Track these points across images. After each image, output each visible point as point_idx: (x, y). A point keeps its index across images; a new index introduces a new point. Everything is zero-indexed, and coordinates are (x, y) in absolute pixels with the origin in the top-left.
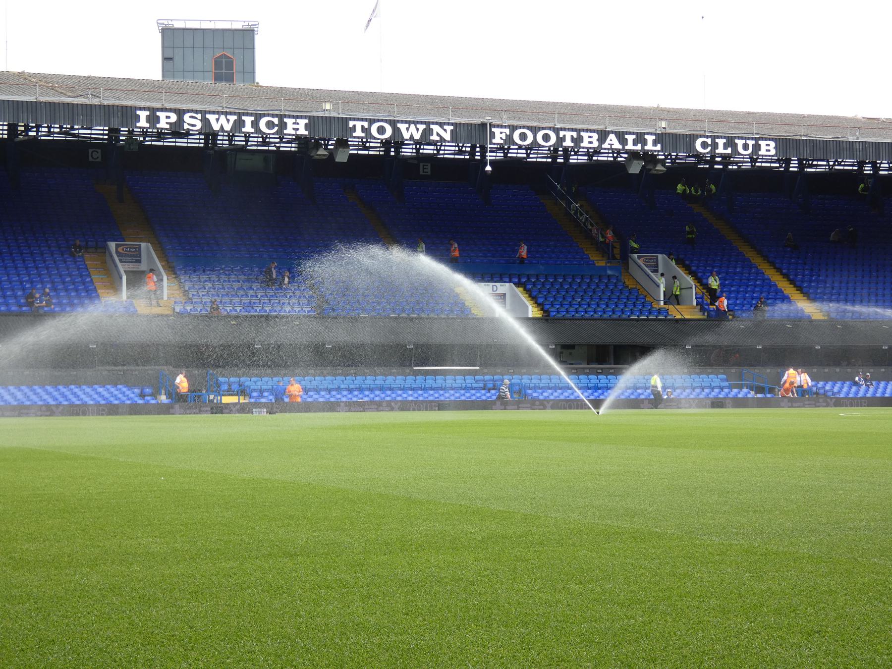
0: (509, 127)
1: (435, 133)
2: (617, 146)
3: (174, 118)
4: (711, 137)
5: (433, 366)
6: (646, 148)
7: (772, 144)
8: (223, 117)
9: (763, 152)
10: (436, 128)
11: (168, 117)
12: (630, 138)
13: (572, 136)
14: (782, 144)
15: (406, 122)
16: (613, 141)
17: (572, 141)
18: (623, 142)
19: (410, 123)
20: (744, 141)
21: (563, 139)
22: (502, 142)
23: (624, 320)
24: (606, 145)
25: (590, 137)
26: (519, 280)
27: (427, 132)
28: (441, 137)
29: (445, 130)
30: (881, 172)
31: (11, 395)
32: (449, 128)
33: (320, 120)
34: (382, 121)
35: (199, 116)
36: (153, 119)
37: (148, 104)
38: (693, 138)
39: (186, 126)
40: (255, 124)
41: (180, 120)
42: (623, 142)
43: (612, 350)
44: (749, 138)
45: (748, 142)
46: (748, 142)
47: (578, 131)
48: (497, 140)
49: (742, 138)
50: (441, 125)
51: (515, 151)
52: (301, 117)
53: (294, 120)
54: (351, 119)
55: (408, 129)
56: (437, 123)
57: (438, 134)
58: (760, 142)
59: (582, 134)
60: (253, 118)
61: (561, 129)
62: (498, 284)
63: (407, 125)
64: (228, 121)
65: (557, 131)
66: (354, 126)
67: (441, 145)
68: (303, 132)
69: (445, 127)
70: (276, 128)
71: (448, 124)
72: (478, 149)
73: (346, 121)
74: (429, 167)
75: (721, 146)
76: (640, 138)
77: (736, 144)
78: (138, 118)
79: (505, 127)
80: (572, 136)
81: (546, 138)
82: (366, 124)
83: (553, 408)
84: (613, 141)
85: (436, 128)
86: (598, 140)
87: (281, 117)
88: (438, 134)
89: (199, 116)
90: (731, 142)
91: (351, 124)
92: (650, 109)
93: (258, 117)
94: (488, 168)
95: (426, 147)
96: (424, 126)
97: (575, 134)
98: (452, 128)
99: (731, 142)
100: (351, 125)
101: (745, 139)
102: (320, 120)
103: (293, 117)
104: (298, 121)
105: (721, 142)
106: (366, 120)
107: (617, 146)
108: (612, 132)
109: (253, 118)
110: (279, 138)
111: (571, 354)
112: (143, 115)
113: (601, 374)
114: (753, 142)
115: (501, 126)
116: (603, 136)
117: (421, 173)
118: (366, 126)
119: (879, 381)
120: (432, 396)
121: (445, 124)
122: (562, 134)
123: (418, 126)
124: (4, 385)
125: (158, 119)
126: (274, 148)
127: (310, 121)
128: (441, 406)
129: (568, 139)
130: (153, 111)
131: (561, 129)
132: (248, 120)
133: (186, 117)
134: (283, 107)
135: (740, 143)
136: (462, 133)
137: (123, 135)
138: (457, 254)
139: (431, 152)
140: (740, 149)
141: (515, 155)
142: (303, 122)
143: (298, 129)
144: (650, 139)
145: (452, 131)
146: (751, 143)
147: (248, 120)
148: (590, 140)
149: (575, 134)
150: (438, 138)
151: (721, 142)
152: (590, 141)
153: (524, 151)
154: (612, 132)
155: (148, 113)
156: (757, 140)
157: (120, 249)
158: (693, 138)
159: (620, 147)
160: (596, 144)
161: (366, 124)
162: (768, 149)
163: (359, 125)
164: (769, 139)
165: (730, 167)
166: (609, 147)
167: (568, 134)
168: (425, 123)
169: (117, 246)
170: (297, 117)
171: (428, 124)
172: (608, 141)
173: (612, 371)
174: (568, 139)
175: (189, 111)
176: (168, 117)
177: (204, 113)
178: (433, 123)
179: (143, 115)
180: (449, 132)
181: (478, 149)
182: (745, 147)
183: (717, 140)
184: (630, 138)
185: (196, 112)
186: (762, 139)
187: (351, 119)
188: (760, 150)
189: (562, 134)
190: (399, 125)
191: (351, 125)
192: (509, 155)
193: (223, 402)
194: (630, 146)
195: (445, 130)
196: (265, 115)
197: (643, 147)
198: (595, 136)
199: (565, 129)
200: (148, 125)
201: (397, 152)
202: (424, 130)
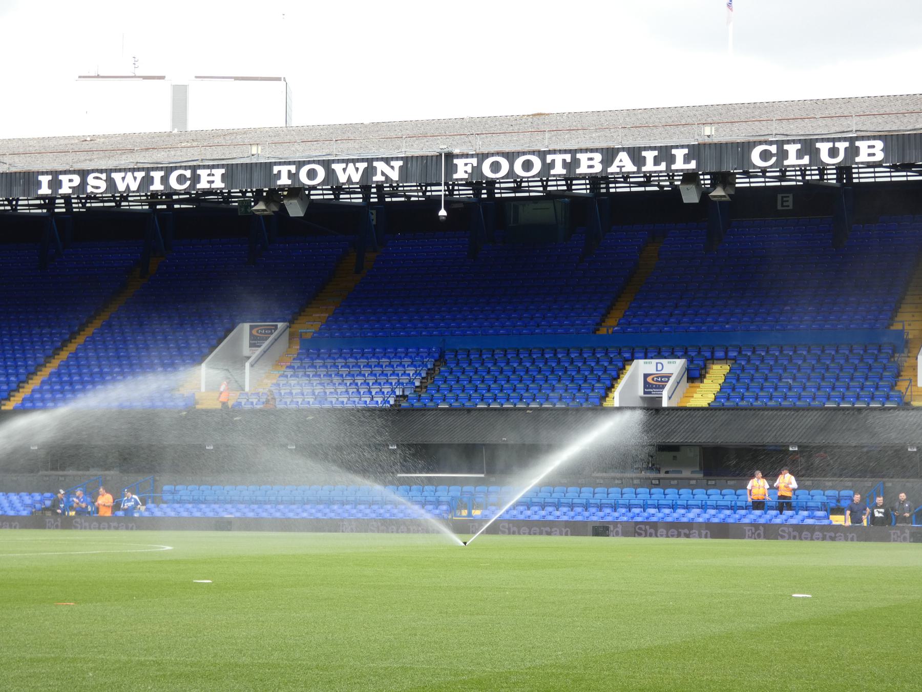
0: (477, 155)
1: (379, 172)
2: (630, 167)
3: (77, 180)
4: (776, 142)
5: (436, 472)
6: (674, 167)
7: (879, 144)
8: (129, 174)
9: (863, 157)
10: (380, 166)
11: (71, 181)
12: (650, 156)
13: (564, 161)
14: (232, 172)
15: (343, 161)
16: (624, 162)
17: (289, 178)
19: (347, 161)
20: (830, 145)
21: (552, 165)
22: (466, 176)
23: (786, 409)
24: (613, 169)
26: (726, 353)
27: (369, 171)
28: (387, 177)
29: (392, 167)
30: (56, 210)
31: (18, 503)
32: (397, 164)
33: (239, 168)
34: (314, 162)
35: (104, 176)
36: (55, 184)
37: (49, 168)
38: (748, 146)
39: (90, 189)
40: (165, 180)
41: (84, 184)
44: (839, 140)
45: (837, 145)
46: (837, 145)
47: (573, 152)
49: (828, 140)
50: (387, 161)
51: (554, 183)
52: (218, 167)
53: (208, 171)
54: (275, 164)
56: (382, 159)
57: (383, 174)
60: (162, 173)
61: (550, 152)
62: (664, 361)
63: (344, 165)
65: (542, 155)
66: (279, 172)
68: (219, 184)
69: (392, 163)
70: (774, 159)
71: (397, 159)
72: (374, 190)
73: (269, 166)
74: (791, 199)
76: (665, 154)
77: (818, 150)
78: (39, 185)
79: (472, 156)
80: (564, 161)
81: (527, 166)
82: (293, 169)
83: (626, 534)
85: (380, 166)
87: (194, 169)
88: (383, 174)
89: (104, 176)
90: (808, 147)
91: (276, 169)
92: (561, 115)
93: (169, 170)
94: (443, 213)
95: (434, 188)
96: (365, 165)
97: (568, 158)
98: (401, 163)
99: (808, 147)
100: (275, 172)
101: (833, 140)
102: (239, 168)
103: (208, 167)
104: (214, 171)
105: (792, 149)
106: (294, 163)
107: (630, 167)
108: (623, 149)
109: (162, 173)
110: (780, 171)
111: (675, 457)
112: (45, 180)
113: (656, 486)
114: (847, 144)
115: (467, 156)
116: (609, 155)
117: (779, 207)
118: (293, 171)
120: (208, 511)
121: (392, 159)
122: (549, 158)
123: (358, 165)
124: (6, 491)
125: (59, 184)
126: (656, 189)
128: (223, 525)
129: (284, 175)
130: (55, 174)
131: (550, 152)
132: (157, 175)
133: (90, 179)
134: (853, 125)
135: (824, 148)
136: (414, 168)
137: (374, 193)
139: (584, 192)
140: (825, 157)
141: (555, 188)
142: (219, 172)
143: (213, 182)
145: (401, 168)
146: (842, 146)
147: (157, 175)
148: (591, 163)
149: (568, 158)
150: (383, 179)
152: (590, 165)
153: (564, 183)
154: (623, 149)
155: (50, 177)
156: (852, 140)
157: (254, 332)
158: (748, 146)
159: (635, 169)
160: (598, 168)
161: (293, 169)
162: (871, 151)
163: (284, 170)
164: (875, 138)
165: (158, 207)
166: (618, 170)
167: (559, 159)
168: (367, 160)
169: (252, 328)
170: (213, 167)
171: (370, 161)
172: (617, 162)
173: (673, 482)
174: (284, 175)
175: (93, 171)
176: (71, 181)
177: (109, 172)
178: (377, 159)
179: (45, 180)
180: (397, 169)
181: (374, 190)
182: (833, 152)
183: (786, 147)
184: (650, 156)
185: (101, 171)
186: (863, 138)
187: (275, 164)
189: (549, 158)
190: (334, 166)
191: (275, 172)
192: (549, 188)
193: (834, 523)
194: (649, 167)
195: (392, 167)
196: (176, 168)
198: (598, 157)
199: (554, 152)
200: (223, 185)
201: (491, 193)
202: (366, 170)
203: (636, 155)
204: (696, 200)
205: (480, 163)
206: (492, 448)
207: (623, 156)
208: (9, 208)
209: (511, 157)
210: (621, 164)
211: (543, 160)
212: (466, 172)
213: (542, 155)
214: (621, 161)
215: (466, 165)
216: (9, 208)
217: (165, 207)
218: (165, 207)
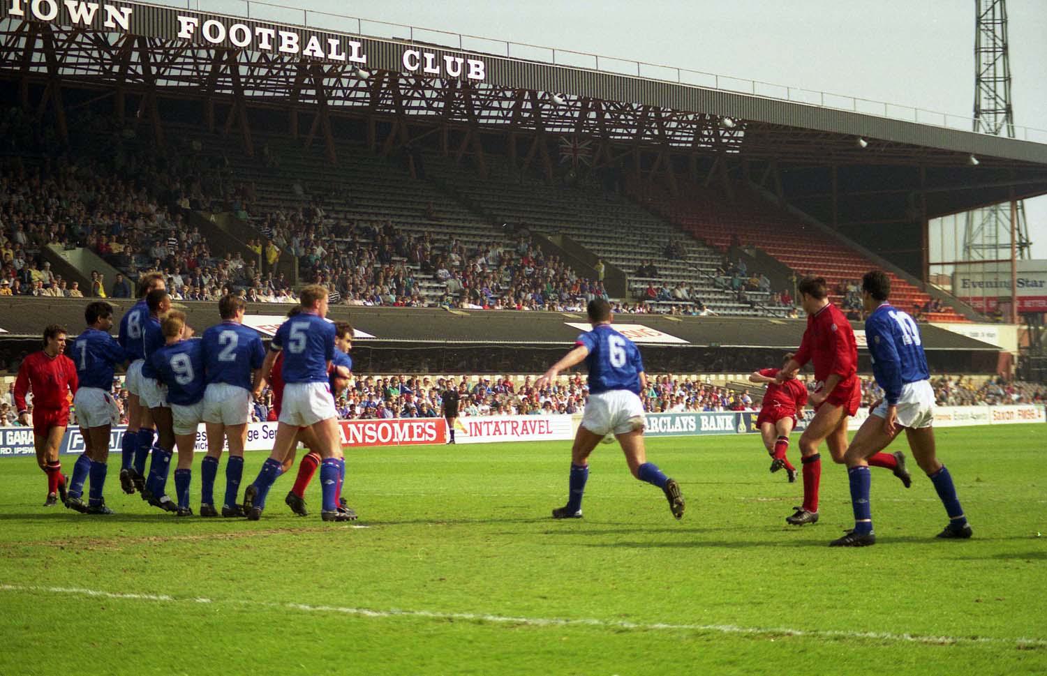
0: (994, 29)
16: (314, 44)
18: (326, 48)
22: (189, 36)
25: (290, 38)
28: (117, 23)
29: (122, 14)
30: (330, 103)
32: (127, 11)
42: (326, 48)
43: (859, 521)
48: (183, 34)
55: (77, 8)
58: (470, 61)
59: (281, 33)
64: (89, 10)
65: (252, 25)
67: (490, 95)
69: (123, 9)
75: (429, 63)
76: (344, 47)
84: (314, 44)
86: (484, 70)
88: (113, 19)
107: (320, 54)
119: (81, 433)
122: (258, 30)
127: (135, 11)
138: (574, 278)
144: (355, 46)
146: (460, 61)
149: (272, 32)
151: (429, 57)
152: (290, 43)
167: (266, 32)
172: (309, 47)
182: (455, 65)
184: (334, 43)
188: (469, 72)
189: (258, 30)
195: (122, 14)
196: (237, 22)
197: (347, 57)
203: (324, 38)
204: (211, 66)
205: (202, 24)
206: (82, 411)
207: (314, 39)
208: (195, 74)
209: (228, 22)
210: (313, 48)
211: (253, 32)
212: (189, 32)
213: (252, 25)
214: (313, 45)
215: (189, 23)
216: (195, 74)
217: (737, 152)
218: (737, 152)
